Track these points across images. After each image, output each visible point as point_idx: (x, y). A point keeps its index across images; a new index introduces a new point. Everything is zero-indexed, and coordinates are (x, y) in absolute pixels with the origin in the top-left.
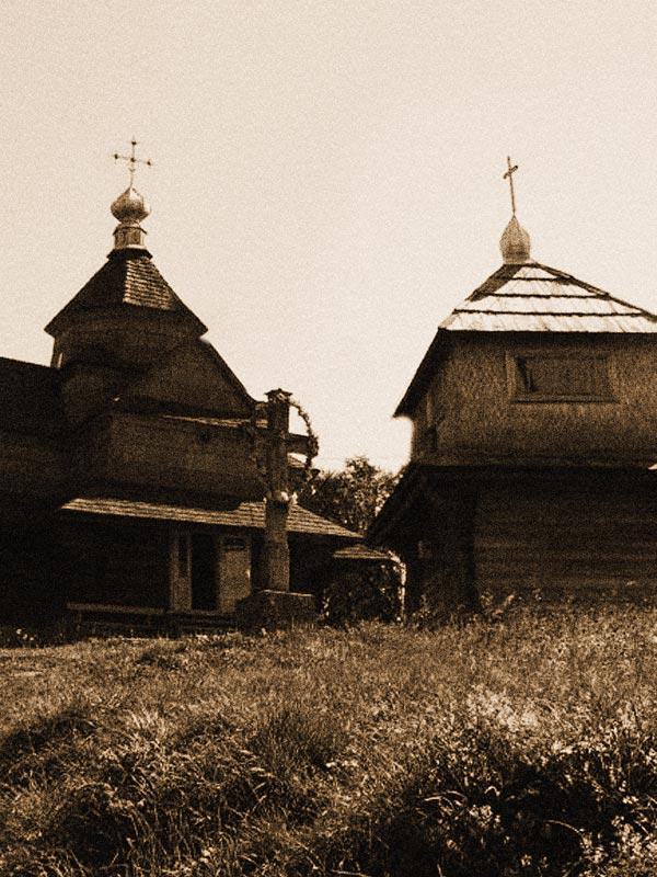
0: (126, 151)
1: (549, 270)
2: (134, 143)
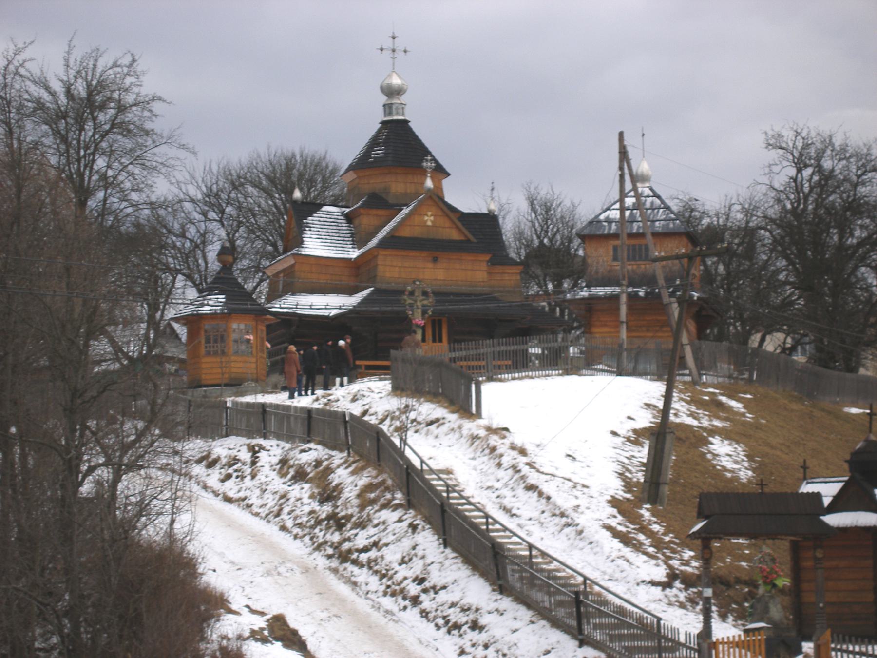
1: (621, 168)
2: (394, 38)
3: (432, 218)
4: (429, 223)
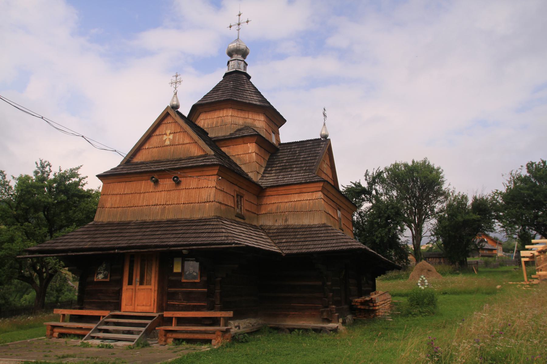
0: (243, 19)
2: (247, 22)
3: (171, 137)
4: (168, 143)
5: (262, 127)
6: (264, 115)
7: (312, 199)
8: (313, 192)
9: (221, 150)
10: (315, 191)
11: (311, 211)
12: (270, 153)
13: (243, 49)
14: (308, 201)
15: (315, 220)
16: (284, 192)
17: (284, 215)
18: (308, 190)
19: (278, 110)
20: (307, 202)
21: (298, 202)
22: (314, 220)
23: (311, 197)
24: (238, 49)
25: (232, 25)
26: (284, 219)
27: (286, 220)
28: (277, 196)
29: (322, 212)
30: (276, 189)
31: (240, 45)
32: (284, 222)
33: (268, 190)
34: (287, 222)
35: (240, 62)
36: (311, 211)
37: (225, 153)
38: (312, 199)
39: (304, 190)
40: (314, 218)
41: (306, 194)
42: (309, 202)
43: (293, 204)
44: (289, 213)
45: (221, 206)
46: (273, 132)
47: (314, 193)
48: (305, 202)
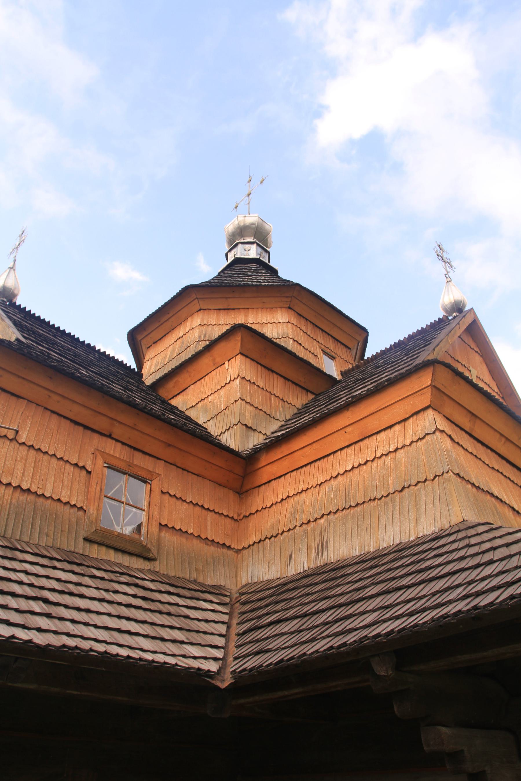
5: (283, 334)
6: (290, 311)
7: (404, 446)
8: (405, 420)
9: (169, 404)
10: (412, 415)
11: (404, 488)
12: (312, 393)
13: (253, 224)
14: (390, 456)
15: (423, 519)
16: (310, 454)
17: (314, 530)
18: (387, 418)
19: (343, 312)
20: (388, 460)
21: (356, 471)
22: (417, 520)
23: (401, 440)
24: (242, 224)
25: (238, 202)
26: (314, 545)
27: (322, 547)
28: (294, 473)
29: (449, 480)
30: (285, 449)
31: (246, 218)
32: (313, 556)
33: (264, 459)
34: (325, 553)
35: (247, 246)
36: (404, 488)
37: (177, 408)
38: (404, 446)
39: (374, 424)
40: (417, 513)
41: (382, 434)
42: (394, 459)
43: (343, 483)
44: (332, 516)
45: (35, 503)
46: (325, 353)
47: (410, 421)
48: (381, 462)
